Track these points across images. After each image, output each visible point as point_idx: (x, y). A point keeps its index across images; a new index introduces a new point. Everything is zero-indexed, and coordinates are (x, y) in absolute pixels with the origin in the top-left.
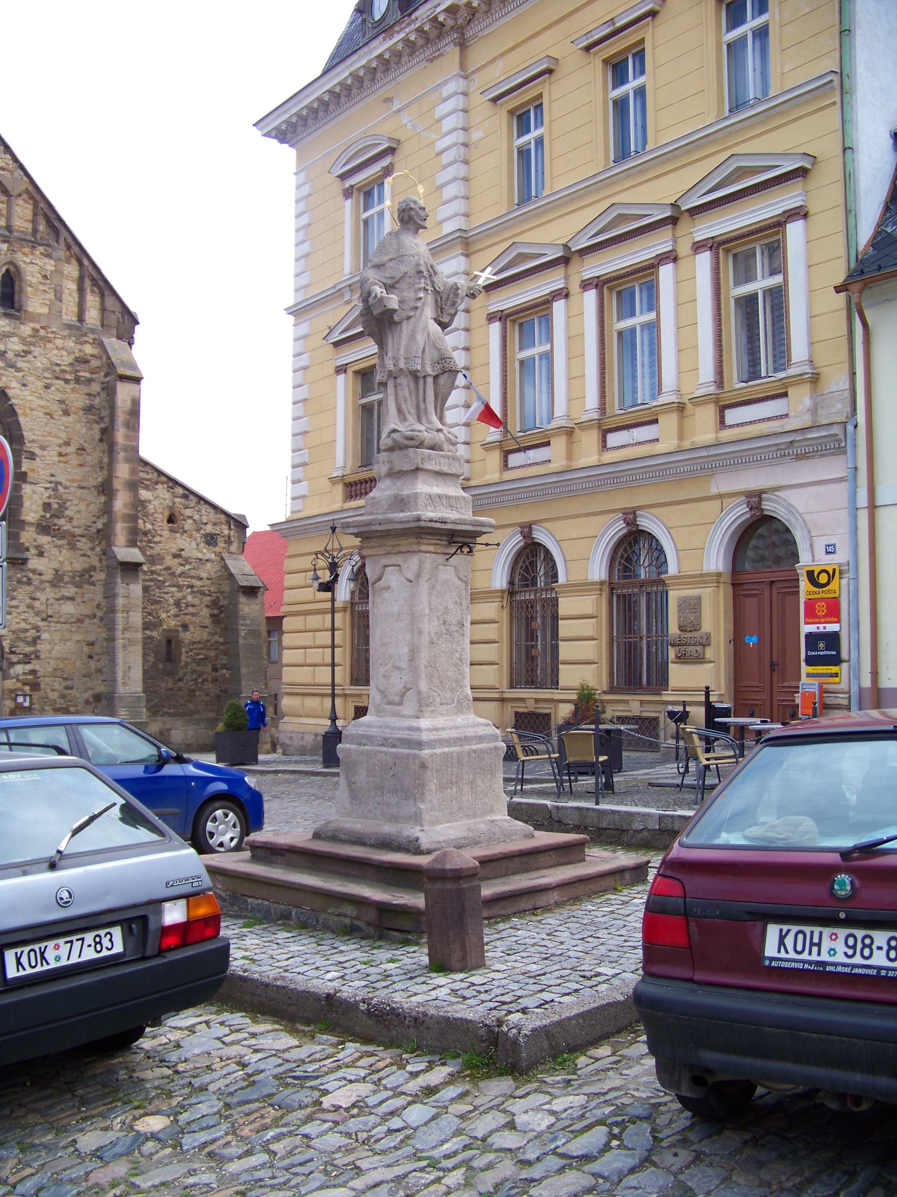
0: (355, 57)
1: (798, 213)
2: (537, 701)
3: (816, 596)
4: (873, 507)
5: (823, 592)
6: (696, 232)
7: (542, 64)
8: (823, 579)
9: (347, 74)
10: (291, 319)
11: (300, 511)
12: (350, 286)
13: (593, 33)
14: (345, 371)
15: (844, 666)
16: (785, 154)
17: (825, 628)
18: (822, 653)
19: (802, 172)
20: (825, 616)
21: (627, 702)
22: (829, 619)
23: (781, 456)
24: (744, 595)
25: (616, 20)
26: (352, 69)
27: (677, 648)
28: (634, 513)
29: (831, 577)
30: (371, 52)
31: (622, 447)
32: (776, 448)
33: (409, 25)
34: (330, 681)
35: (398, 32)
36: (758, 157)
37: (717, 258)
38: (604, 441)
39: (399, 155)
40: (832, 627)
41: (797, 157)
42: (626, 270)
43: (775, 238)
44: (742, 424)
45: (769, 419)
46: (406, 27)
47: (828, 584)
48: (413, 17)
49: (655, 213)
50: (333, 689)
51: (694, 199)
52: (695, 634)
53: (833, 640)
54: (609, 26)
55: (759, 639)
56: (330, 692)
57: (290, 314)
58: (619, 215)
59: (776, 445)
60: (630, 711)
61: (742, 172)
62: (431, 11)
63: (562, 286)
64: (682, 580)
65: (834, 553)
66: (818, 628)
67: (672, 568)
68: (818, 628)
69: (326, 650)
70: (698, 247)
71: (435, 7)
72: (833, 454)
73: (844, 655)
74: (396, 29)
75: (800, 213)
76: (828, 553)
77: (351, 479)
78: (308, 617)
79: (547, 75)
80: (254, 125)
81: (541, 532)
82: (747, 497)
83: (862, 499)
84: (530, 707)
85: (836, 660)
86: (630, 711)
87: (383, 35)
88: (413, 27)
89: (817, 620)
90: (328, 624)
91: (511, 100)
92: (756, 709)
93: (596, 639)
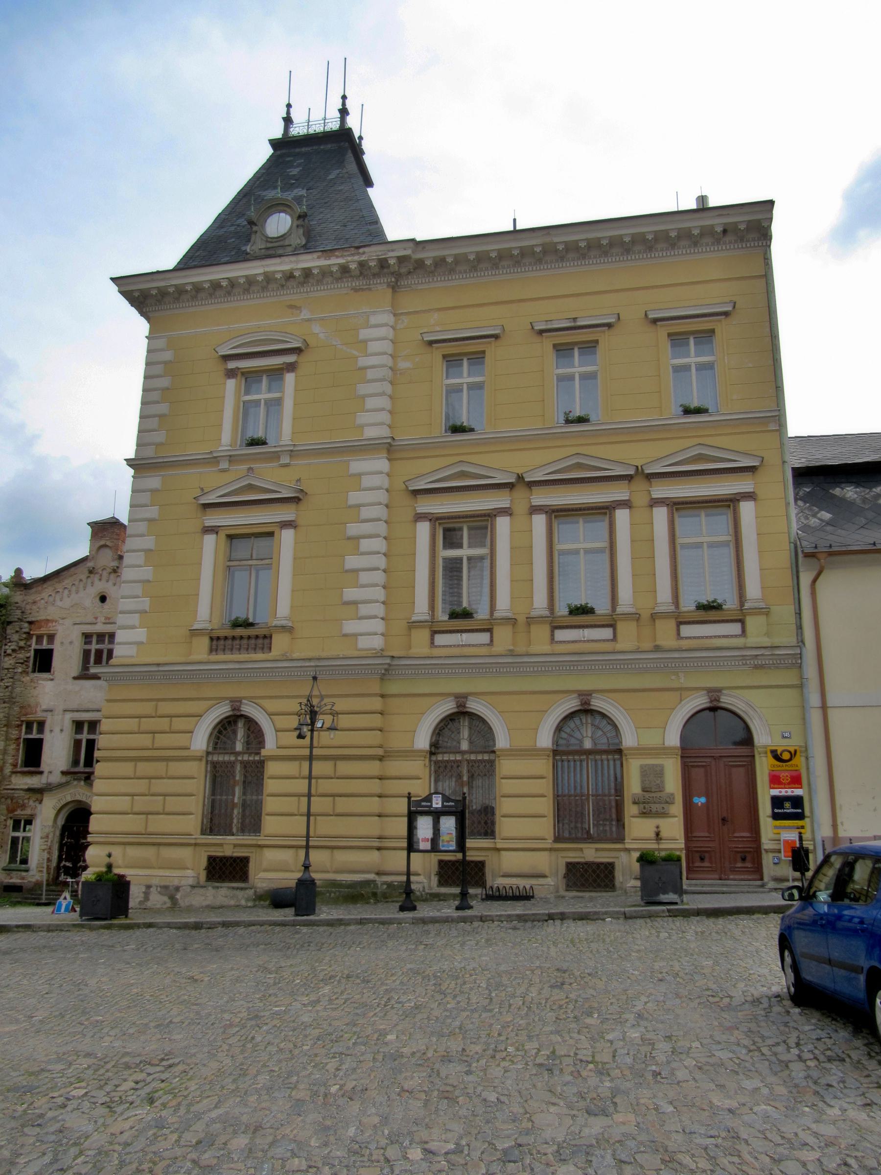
0: (277, 260)
1: (507, 512)
2: (235, 846)
3: (779, 768)
4: (824, 707)
5: (786, 766)
6: (206, 519)
7: (495, 330)
8: (786, 756)
9: (261, 271)
10: (131, 472)
11: (133, 657)
12: (230, 456)
13: (553, 322)
14: (217, 533)
15: (807, 820)
16: (746, 454)
17: (792, 792)
18: (788, 811)
19: (752, 469)
20: (789, 784)
21: (581, 850)
22: (793, 786)
23: (744, 665)
24: (693, 766)
25: (578, 319)
26: (267, 269)
27: (642, 806)
28: (240, 702)
29: (793, 755)
30: (297, 262)
31: (573, 642)
32: (741, 658)
33: (353, 255)
34: (304, 833)
35: (337, 257)
36: (586, 457)
37: (435, 529)
38: (552, 635)
39: (303, 359)
40: (798, 792)
41: (511, 474)
42: (580, 506)
43: (484, 523)
44: (698, 638)
45: (724, 636)
46: (348, 256)
47: (790, 760)
48: (361, 250)
49: (283, 491)
50: (308, 841)
51: (422, 483)
52: (658, 794)
53: (797, 802)
54: (570, 322)
55: (707, 802)
56: (304, 843)
57: (130, 465)
58: (578, 463)
59: (743, 656)
60: (224, 852)
61: (463, 475)
62: (383, 253)
63: (508, 506)
64: (641, 751)
65: (790, 738)
66: (780, 792)
67: (502, 741)
68: (780, 792)
69: (302, 798)
70: (535, 510)
71: (389, 251)
72: (787, 668)
73: (807, 812)
74: (337, 253)
75: (750, 496)
76: (783, 737)
77: (215, 634)
78: (170, 764)
79: (493, 339)
80: (112, 279)
81: (250, 705)
82: (231, 701)
83: (814, 699)
84: (228, 852)
85: (800, 816)
86: (584, 858)
87: (320, 254)
88: (356, 258)
89: (782, 786)
90: (306, 772)
91: (708, 322)
92: (707, 855)
93: (545, 796)
